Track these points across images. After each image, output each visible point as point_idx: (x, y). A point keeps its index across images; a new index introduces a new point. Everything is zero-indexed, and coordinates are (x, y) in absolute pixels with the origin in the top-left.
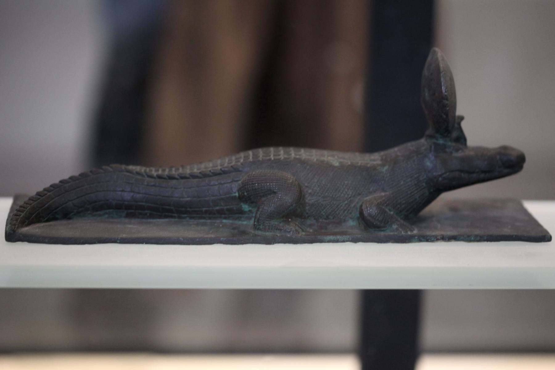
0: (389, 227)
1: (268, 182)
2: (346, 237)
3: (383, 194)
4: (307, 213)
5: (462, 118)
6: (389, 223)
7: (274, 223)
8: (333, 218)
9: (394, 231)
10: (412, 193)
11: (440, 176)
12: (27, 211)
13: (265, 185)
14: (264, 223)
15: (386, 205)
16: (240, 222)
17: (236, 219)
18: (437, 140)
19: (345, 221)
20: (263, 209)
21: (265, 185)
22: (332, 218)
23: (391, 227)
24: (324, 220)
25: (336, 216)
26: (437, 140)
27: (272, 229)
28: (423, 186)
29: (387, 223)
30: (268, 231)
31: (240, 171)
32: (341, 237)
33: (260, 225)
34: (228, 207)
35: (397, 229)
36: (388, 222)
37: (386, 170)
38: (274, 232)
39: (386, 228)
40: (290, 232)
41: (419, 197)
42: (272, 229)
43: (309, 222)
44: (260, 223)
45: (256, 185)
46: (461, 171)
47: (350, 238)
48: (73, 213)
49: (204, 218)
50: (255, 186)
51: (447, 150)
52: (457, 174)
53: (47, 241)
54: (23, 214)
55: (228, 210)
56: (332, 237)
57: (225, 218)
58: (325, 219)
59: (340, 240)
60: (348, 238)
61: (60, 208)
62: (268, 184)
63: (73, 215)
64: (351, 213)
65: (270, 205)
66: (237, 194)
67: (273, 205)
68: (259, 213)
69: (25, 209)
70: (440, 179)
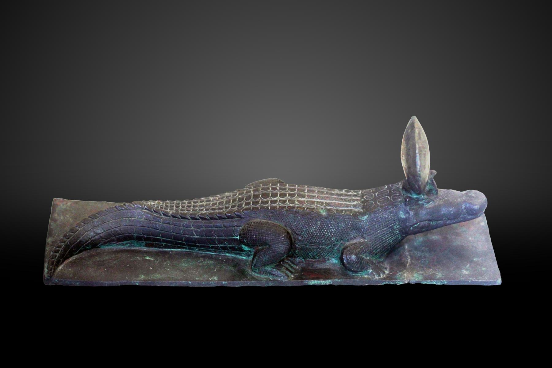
0: (365, 271)
1: (264, 236)
2: (328, 281)
4: (297, 255)
6: (365, 268)
7: (268, 268)
8: (319, 258)
9: (368, 275)
10: (386, 239)
11: (412, 226)
12: (62, 251)
13: (262, 237)
14: (259, 268)
15: (364, 245)
16: (241, 257)
17: (237, 254)
18: (411, 195)
19: (328, 259)
20: (259, 257)
21: (262, 237)
22: (318, 258)
23: (367, 271)
25: (321, 256)
26: (411, 195)
27: (266, 274)
28: (396, 233)
29: (363, 269)
30: (262, 275)
31: (242, 218)
32: (323, 281)
34: (231, 246)
35: (372, 273)
36: (364, 267)
37: (366, 219)
38: (268, 276)
39: (362, 272)
40: (281, 277)
41: (393, 241)
42: (266, 274)
44: (256, 269)
45: (254, 236)
46: (430, 220)
47: (331, 282)
48: (100, 244)
49: (211, 251)
51: (420, 202)
52: (427, 222)
54: (58, 255)
55: (230, 248)
57: (228, 252)
58: (312, 259)
60: (330, 282)
62: (264, 237)
63: (100, 245)
64: (334, 254)
65: (265, 255)
66: (238, 237)
67: (267, 256)
68: (256, 260)
69: (60, 249)
70: (412, 228)
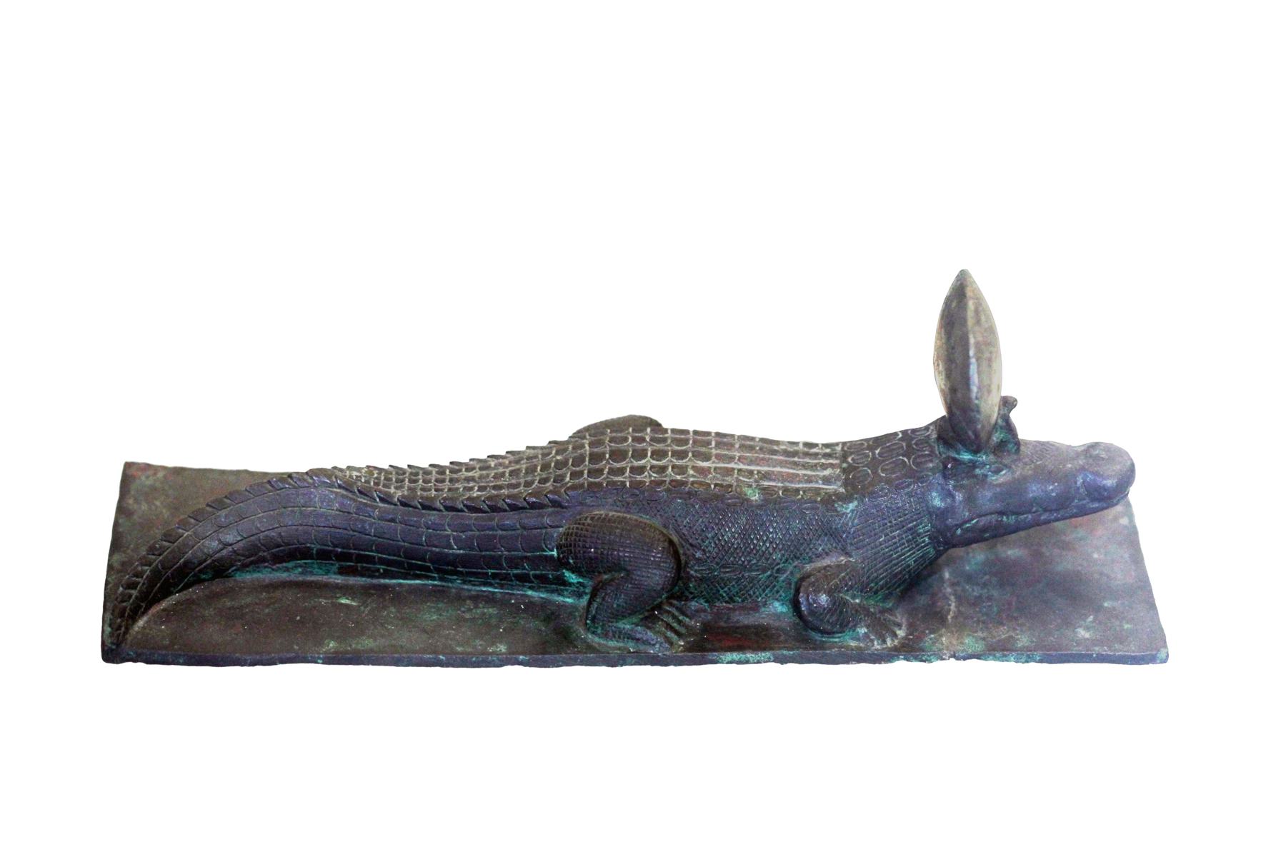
0: (849, 631)
1: (616, 550)
2: (763, 654)
4: (691, 593)
5: (1009, 404)
6: (851, 624)
8: (743, 601)
9: (858, 639)
10: (900, 556)
11: (960, 526)
13: (610, 553)
14: (603, 625)
16: (561, 599)
17: (552, 592)
18: (959, 454)
19: (765, 604)
21: (610, 553)
22: (740, 600)
23: (854, 631)
24: (724, 604)
25: (748, 597)
26: (959, 454)
28: (924, 542)
29: (846, 626)
30: (611, 640)
31: (563, 507)
32: (753, 656)
33: (597, 628)
34: (538, 572)
35: (866, 636)
36: (849, 622)
37: (852, 511)
39: (844, 634)
40: (654, 645)
41: (915, 561)
42: (619, 637)
44: (596, 625)
45: (592, 550)
46: (1001, 513)
48: (234, 568)
51: (978, 471)
52: (994, 518)
53: (181, 661)
54: (134, 593)
55: (536, 577)
56: (735, 656)
57: (531, 588)
59: (751, 660)
60: (768, 656)
61: (209, 562)
62: (616, 553)
63: (233, 571)
65: (616, 594)
68: (596, 606)
69: (140, 580)
70: (959, 531)
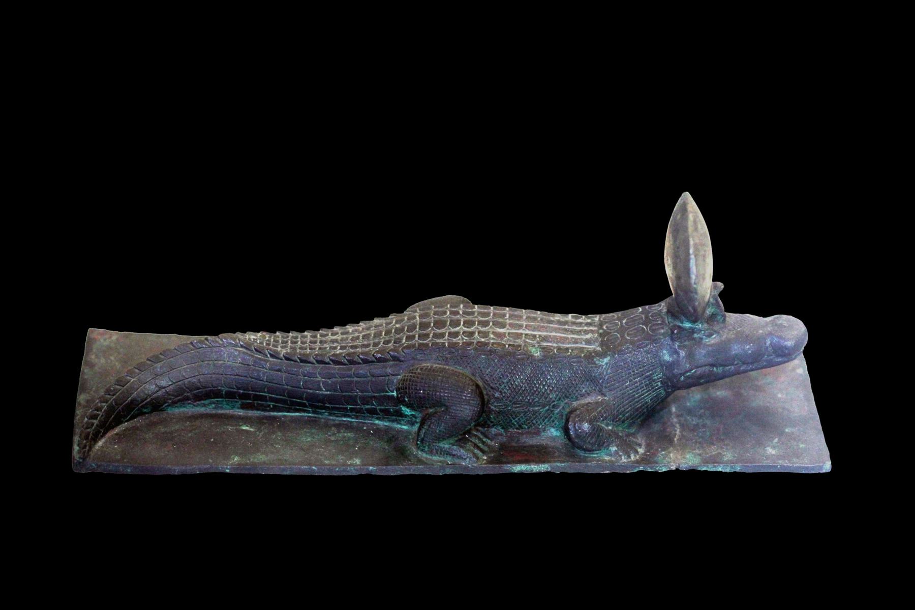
0: (604, 449)
2: (543, 466)
3: (600, 398)
4: (492, 422)
6: (605, 444)
7: (445, 445)
8: (529, 428)
9: (611, 455)
10: (641, 396)
11: (683, 374)
13: (434, 393)
14: (429, 445)
16: (399, 426)
17: (393, 421)
18: (682, 323)
19: (544, 430)
21: (434, 393)
23: (608, 449)
25: (532, 425)
26: (682, 323)
27: (441, 454)
28: (657, 385)
29: (602, 445)
30: (435, 455)
31: (400, 361)
32: (536, 467)
33: (425, 447)
34: (383, 407)
35: (616, 452)
36: (604, 443)
37: (606, 364)
39: (600, 451)
40: (465, 459)
41: (651, 400)
42: (441, 454)
43: (493, 430)
44: (424, 445)
45: (422, 391)
46: (712, 365)
47: (549, 468)
48: (166, 404)
49: (349, 416)
50: (420, 393)
51: (696, 335)
52: (707, 368)
54: (96, 422)
55: (381, 410)
57: (378, 419)
58: (517, 429)
60: (546, 467)
61: (148, 400)
62: (438, 393)
63: (166, 407)
64: (553, 421)
65: (439, 423)
67: (443, 425)
68: (424, 431)
69: (99, 413)
70: (682, 378)
